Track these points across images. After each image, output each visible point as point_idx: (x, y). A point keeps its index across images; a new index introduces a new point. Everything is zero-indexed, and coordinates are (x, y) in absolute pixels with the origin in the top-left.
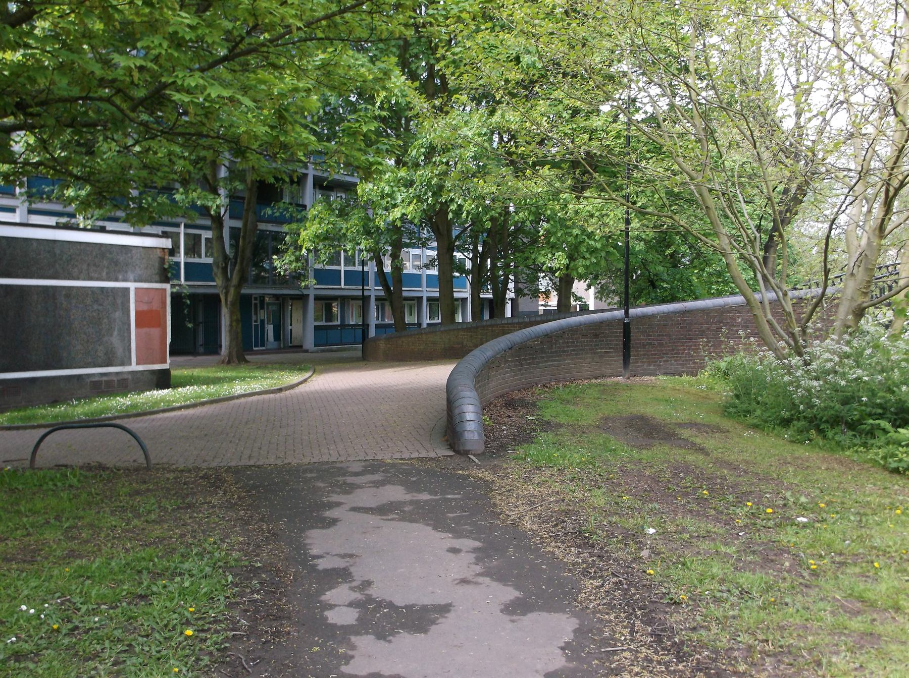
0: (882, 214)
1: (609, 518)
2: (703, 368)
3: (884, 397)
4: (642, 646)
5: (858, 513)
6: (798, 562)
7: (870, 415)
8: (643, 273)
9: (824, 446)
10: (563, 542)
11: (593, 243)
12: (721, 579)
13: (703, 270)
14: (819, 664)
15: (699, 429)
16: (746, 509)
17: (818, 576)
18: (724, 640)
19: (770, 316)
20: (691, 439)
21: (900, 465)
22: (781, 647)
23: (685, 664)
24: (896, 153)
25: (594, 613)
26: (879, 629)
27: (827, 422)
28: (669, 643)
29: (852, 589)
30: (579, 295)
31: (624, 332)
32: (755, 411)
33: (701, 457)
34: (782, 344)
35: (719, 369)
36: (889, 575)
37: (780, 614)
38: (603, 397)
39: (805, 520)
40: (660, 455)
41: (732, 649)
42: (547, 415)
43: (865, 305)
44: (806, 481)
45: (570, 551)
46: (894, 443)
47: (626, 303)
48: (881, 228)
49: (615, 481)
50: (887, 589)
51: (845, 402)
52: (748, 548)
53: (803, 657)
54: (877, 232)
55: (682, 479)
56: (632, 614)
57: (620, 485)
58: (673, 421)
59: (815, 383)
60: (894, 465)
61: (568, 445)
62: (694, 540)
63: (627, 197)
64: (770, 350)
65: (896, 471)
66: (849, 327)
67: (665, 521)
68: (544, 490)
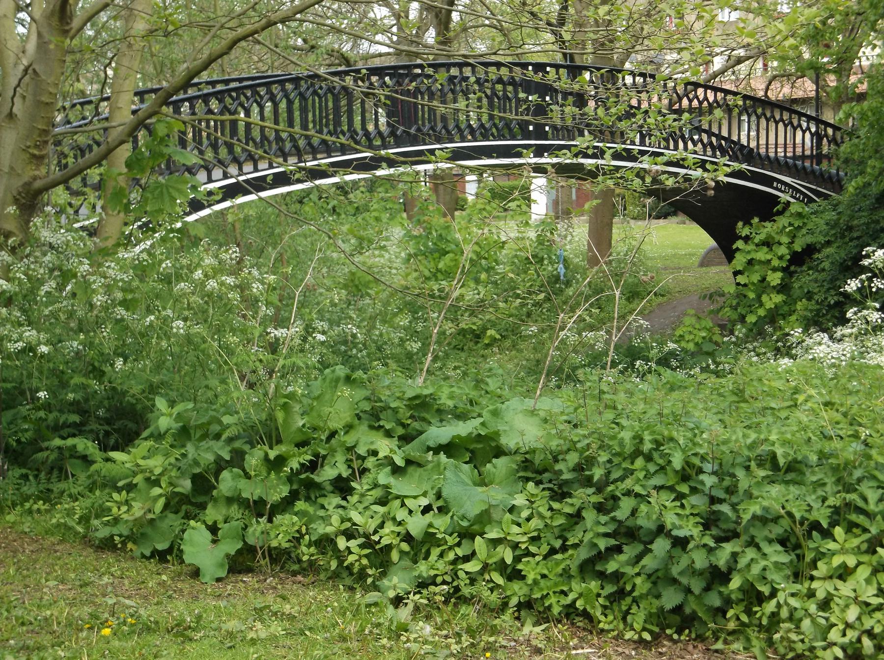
3: (84, 387)
43: (38, 184)
46: (104, 486)
54: (55, 22)
60: (103, 533)
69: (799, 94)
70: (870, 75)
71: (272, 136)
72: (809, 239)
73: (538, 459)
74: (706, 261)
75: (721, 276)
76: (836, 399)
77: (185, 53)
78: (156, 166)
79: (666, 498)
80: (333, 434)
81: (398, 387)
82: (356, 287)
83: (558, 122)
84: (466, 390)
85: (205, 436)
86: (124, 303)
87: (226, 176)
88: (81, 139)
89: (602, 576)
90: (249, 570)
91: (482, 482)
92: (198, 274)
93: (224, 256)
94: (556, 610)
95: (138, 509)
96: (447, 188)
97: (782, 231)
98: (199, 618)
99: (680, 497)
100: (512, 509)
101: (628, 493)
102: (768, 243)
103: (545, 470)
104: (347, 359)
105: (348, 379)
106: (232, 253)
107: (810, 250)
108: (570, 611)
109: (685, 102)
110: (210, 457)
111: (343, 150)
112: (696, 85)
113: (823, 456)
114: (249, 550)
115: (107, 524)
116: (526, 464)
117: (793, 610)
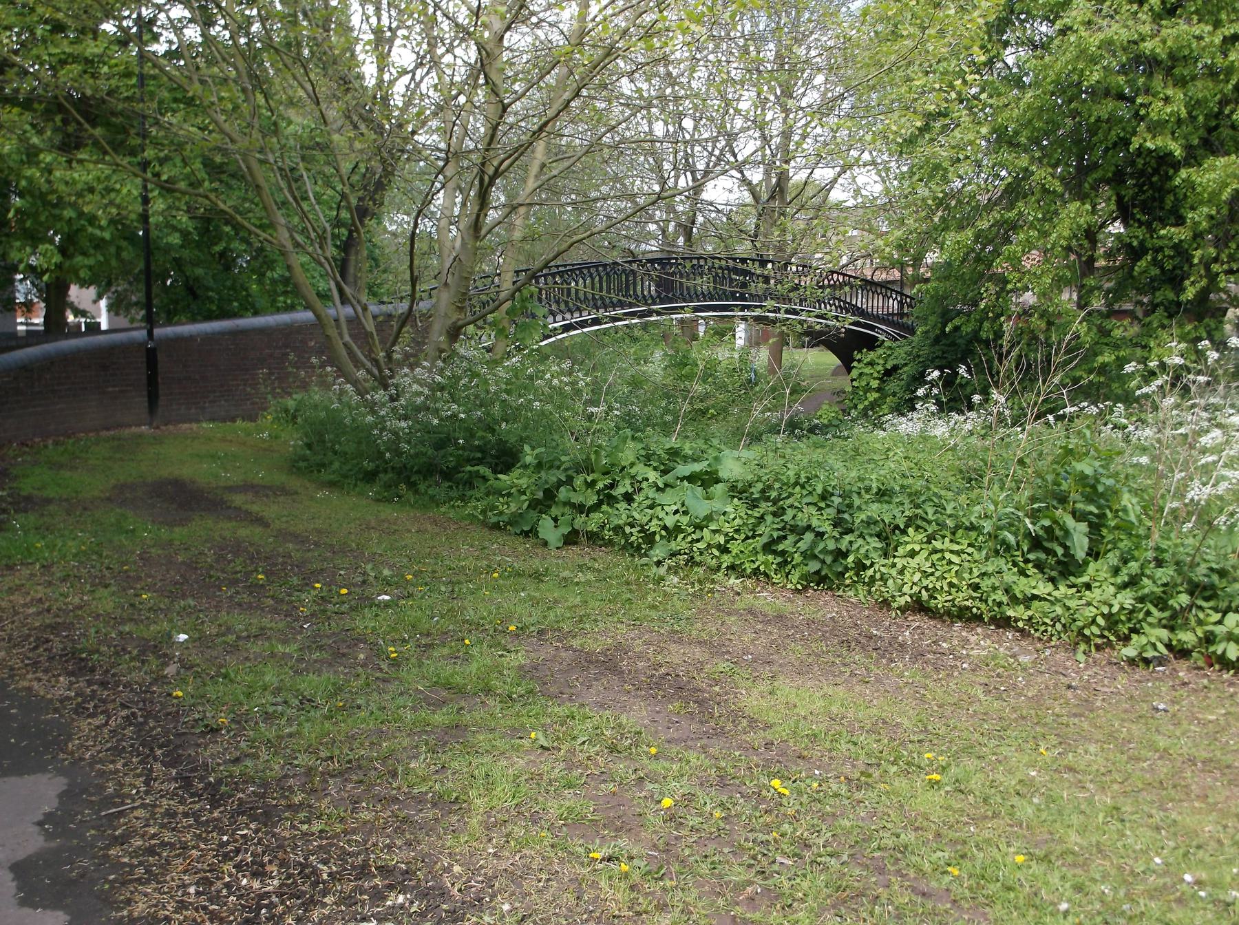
0: (477, 208)
1: (121, 628)
2: (265, 409)
3: (483, 437)
4: (162, 797)
6: (377, 652)
8: (161, 277)
9: (416, 502)
10: (46, 671)
11: (98, 232)
12: (277, 688)
13: (263, 275)
14: (394, 774)
15: (257, 493)
16: (314, 593)
18: (276, 767)
19: (347, 338)
20: (245, 507)
22: (349, 762)
23: (222, 809)
24: (490, 132)
25: (91, 765)
26: (466, 718)
27: (419, 472)
28: (201, 786)
29: (438, 675)
30: (81, 307)
31: (148, 363)
32: (331, 463)
33: (258, 530)
34: (361, 374)
35: (286, 411)
36: (481, 653)
37: (349, 720)
38: (118, 456)
39: (387, 598)
40: (201, 531)
41: (286, 776)
42: (27, 487)
43: (460, 323)
45: (57, 681)
46: (494, 493)
47: (150, 321)
48: (476, 226)
49: (132, 574)
50: (479, 669)
51: (440, 445)
52: (315, 643)
53: (376, 769)
54: (471, 232)
55: (229, 562)
56: (148, 756)
57: (139, 578)
58: (222, 484)
59: (403, 424)
60: (494, 520)
61: (59, 530)
62: (241, 643)
63: (145, 165)
66: (442, 351)
67: (203, 622)
68: (18, 599)
69: (892, 278)
70: (931, 268)
71: (590, 297)
72: (895, 362)
73: (740, 485)
74: (835, 373)
75: (844, 383)
76: (911, 455)
77: (543, 251)
78: (522, 314)
79: (813, 510)
80: (624, 468)
81: (662, 443)
82: (635, 383)
83: (754, 293)
84: (700, 443)
85: (551, 467)
86: (508, 392)
87: (564, 319)
88: (484, 297)
89: (775, 552)
90: (575, 543)
91: (708, 498)
92: (548, 376)
93: (564, 366)
94: (749, 571)
95: (513, 507)
96: (689, 328)
97: (879, 357)
98: (547, 569)
99: (820, 509)
100: (724, 514)
101: (791, 506)
102: (871, 364)
103: (745, 492)
104: (630, 425)
105: (634, 438)
106: (567, 365)
107: (895, 368)
108: (756, 572)
109: (826, 282)
110: (555, 479)
111: (631, 305)
112: (833, 272)
113: (902, 487)
114: (575, 532)
115: (495, 515)
116: (733, 488)
117: (883, 574)
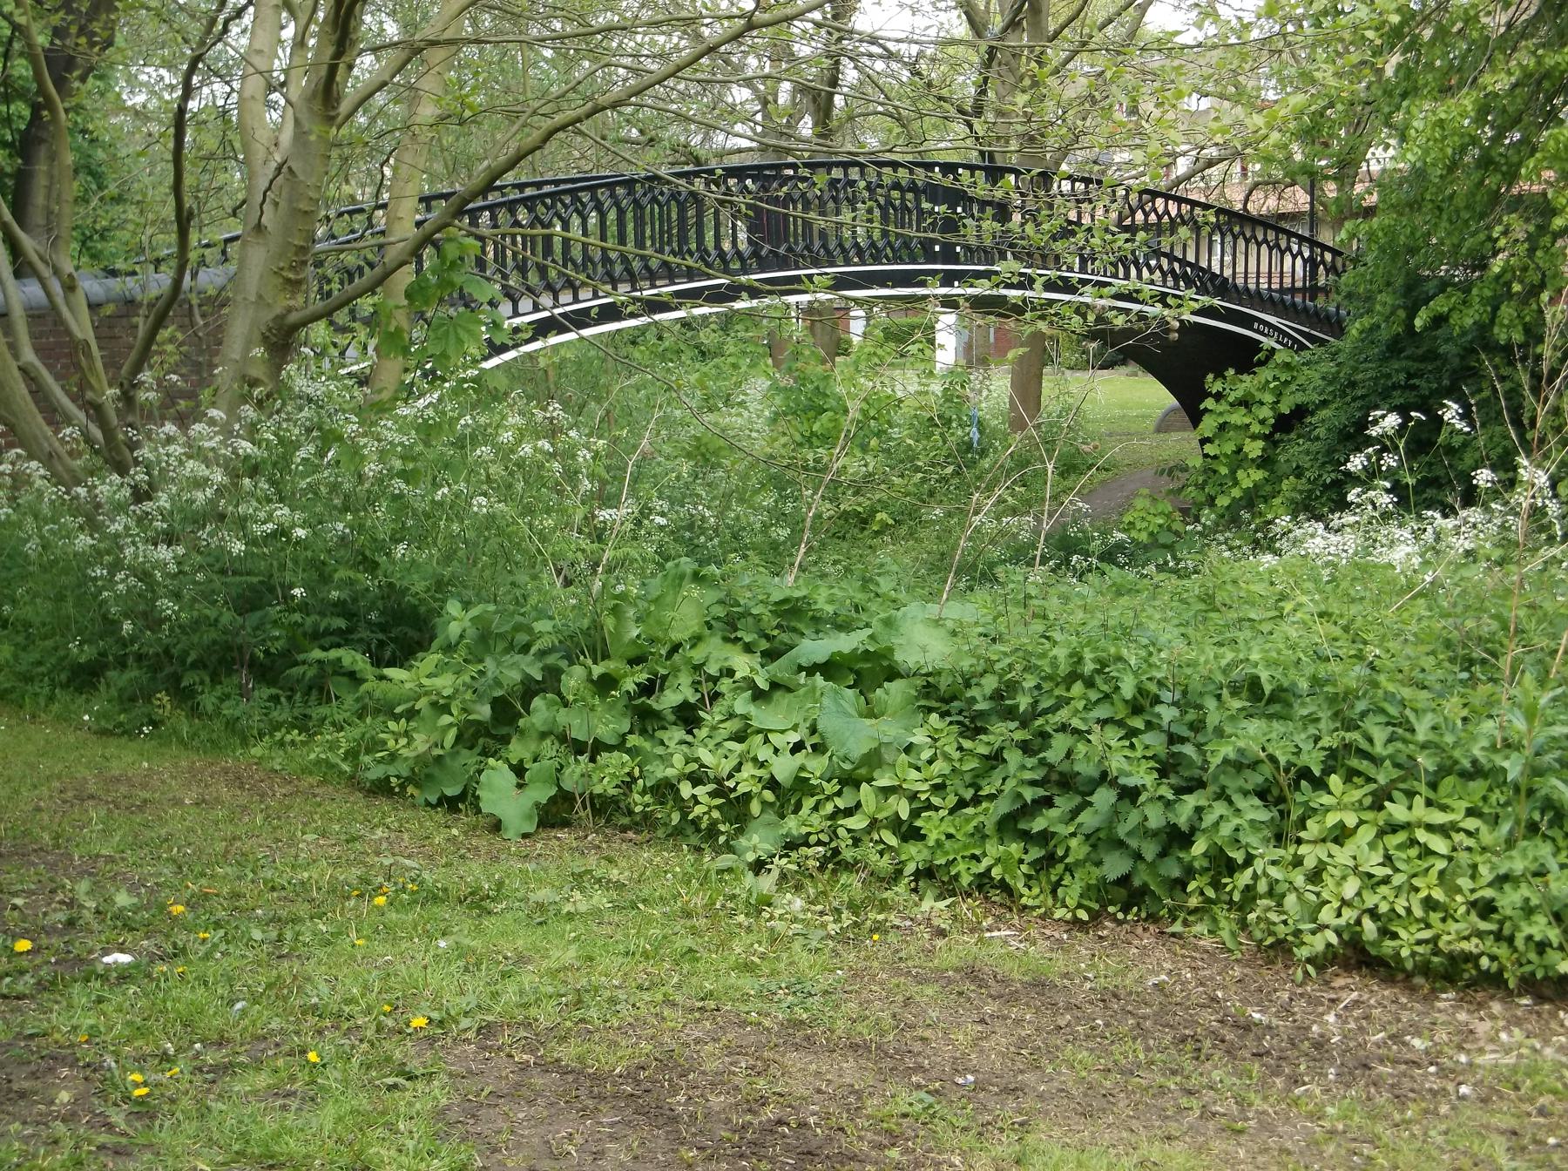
0: (330, 51)
3: (351, 582)
5: (276, 920)
7: (316, 637)
17: (153, 1117)
19: (29, 355)
21: (392, 770)
27: (199, 665)
29: (245, 1137)
39: (125, 958)
43: (293, 317)
44: (137, 845)
46: (377, 712)
48: (327, 93)
50: (340, 1119)
51: (249, 602)
54: (317, 106)
59: (164, 553)
60: (376, 773)
64: (31, 457)
65: (381, 788)
66: (254, 383)
